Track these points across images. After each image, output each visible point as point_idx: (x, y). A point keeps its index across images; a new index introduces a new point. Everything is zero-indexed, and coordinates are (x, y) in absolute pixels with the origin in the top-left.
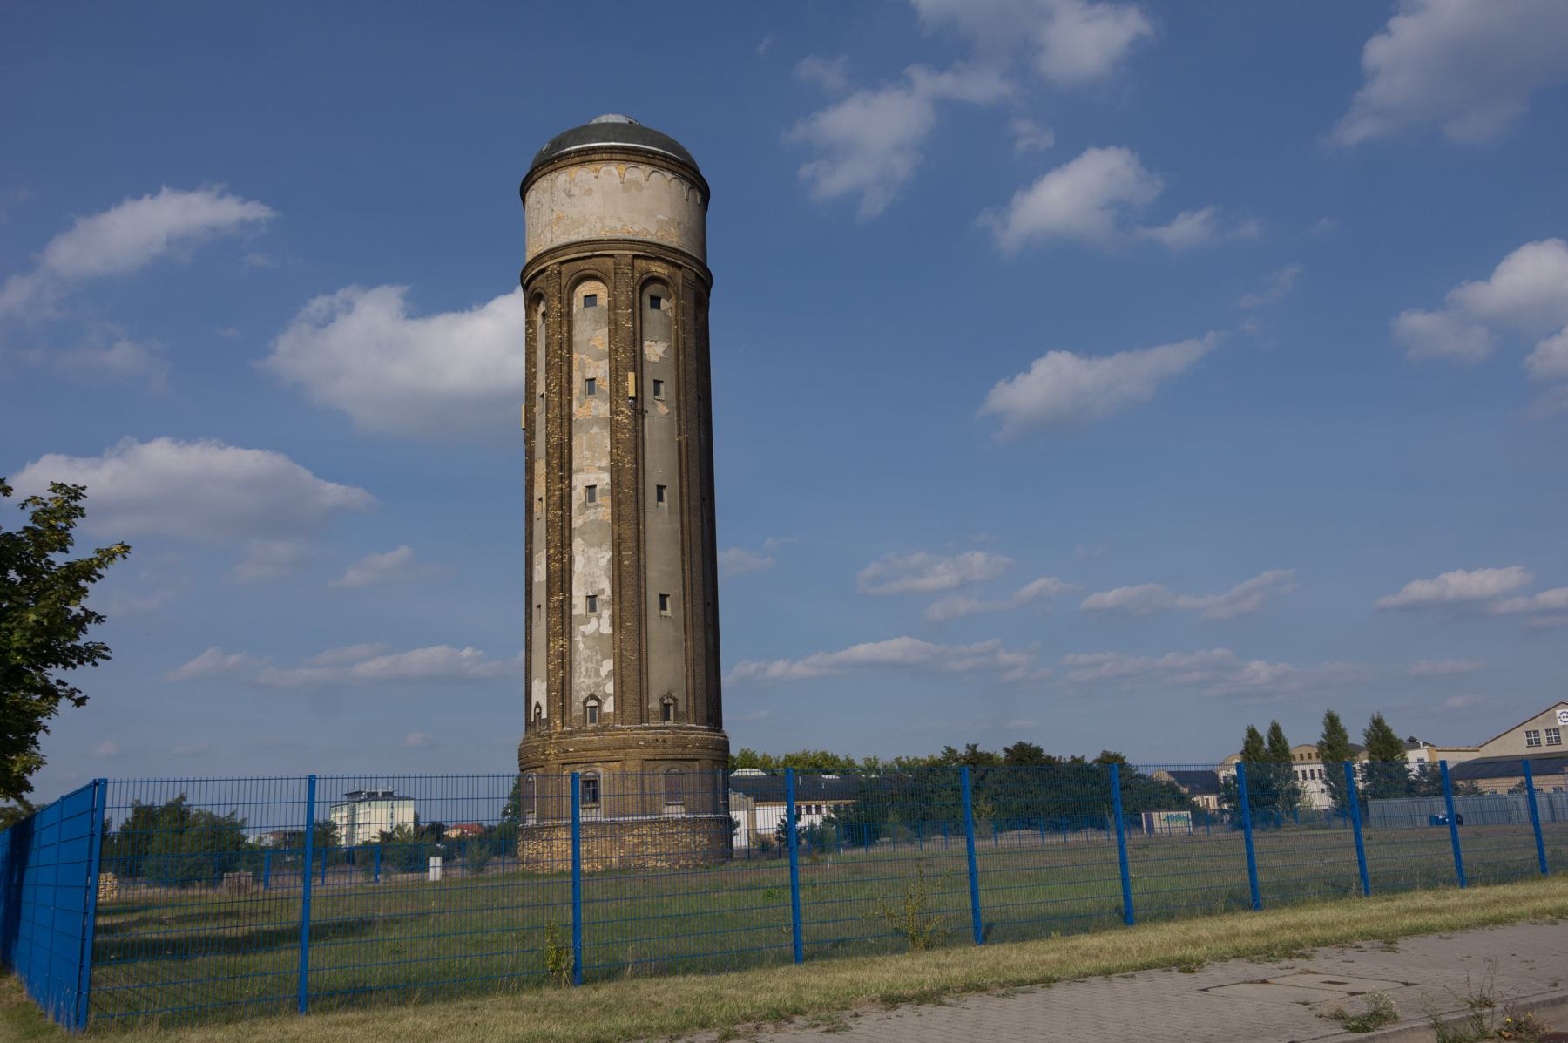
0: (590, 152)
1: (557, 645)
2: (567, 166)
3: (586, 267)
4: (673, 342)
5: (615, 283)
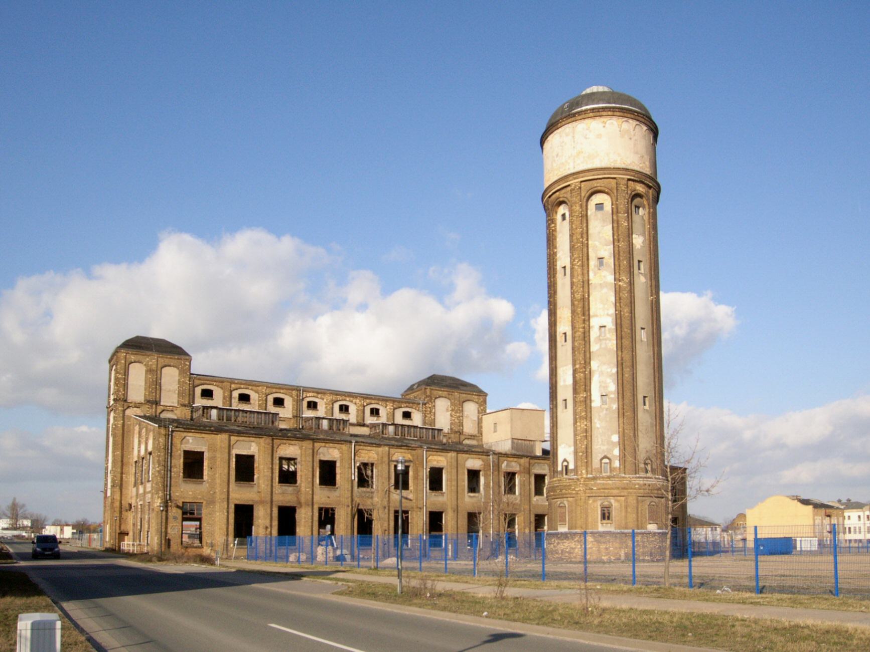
0: (600, 110)
1: (582, 425)
2: (584, 119)
3: (598, 185)
4: (647, 236)
5: (617, 196)
